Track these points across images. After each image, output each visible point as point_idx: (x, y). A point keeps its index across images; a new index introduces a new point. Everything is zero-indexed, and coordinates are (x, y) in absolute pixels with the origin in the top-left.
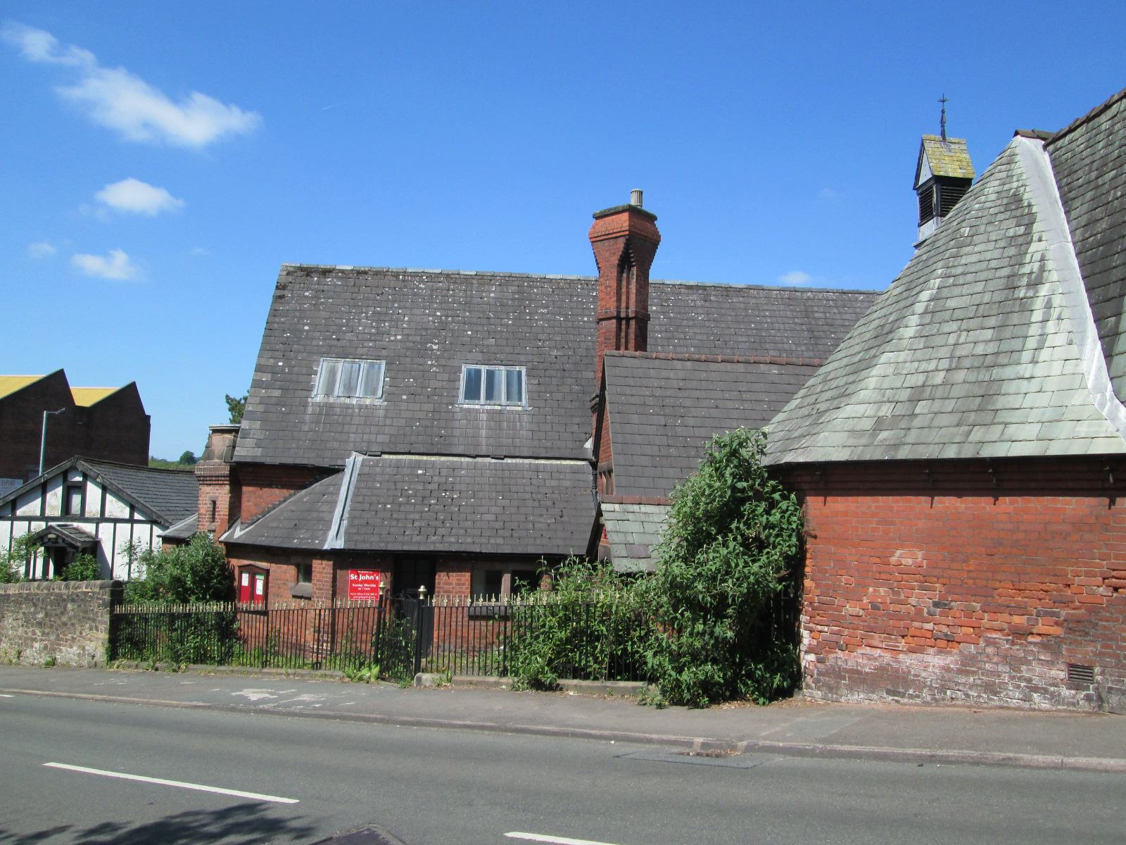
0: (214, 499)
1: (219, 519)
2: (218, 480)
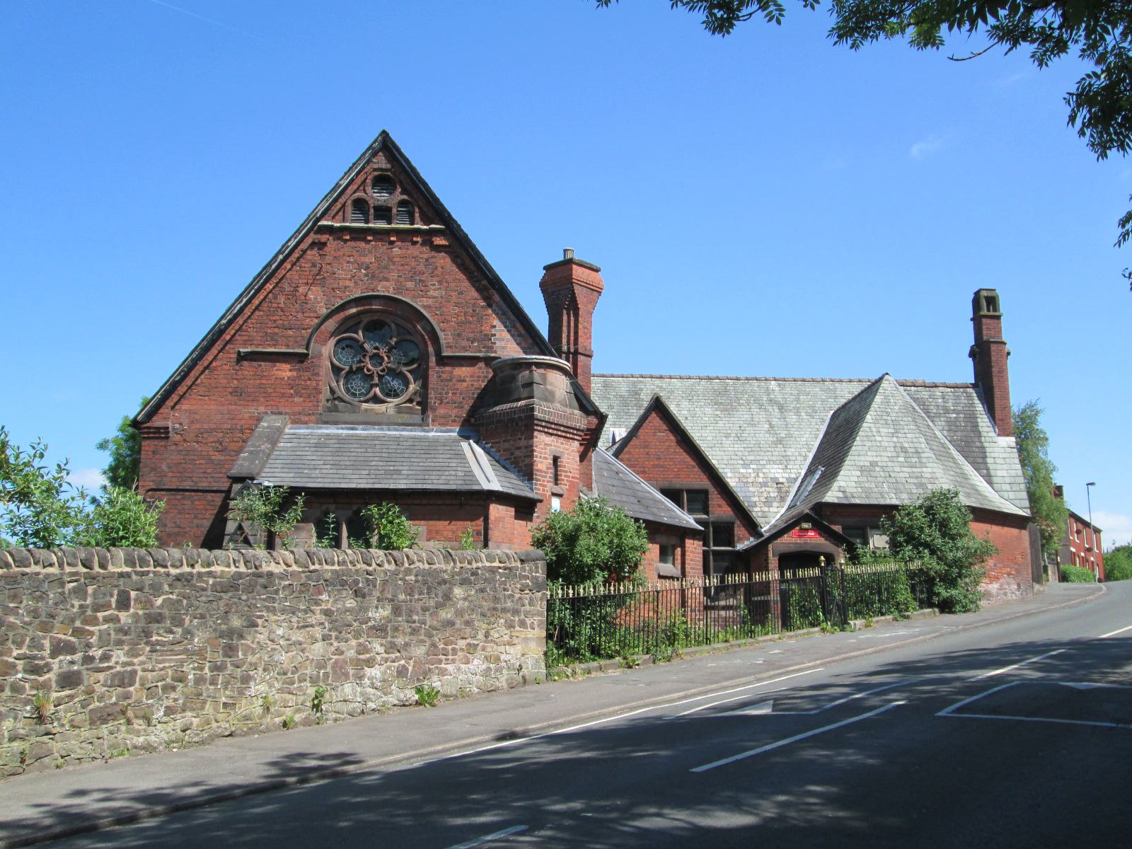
0: (557, 455)
1: (567, 481)
2: (549, 428)
